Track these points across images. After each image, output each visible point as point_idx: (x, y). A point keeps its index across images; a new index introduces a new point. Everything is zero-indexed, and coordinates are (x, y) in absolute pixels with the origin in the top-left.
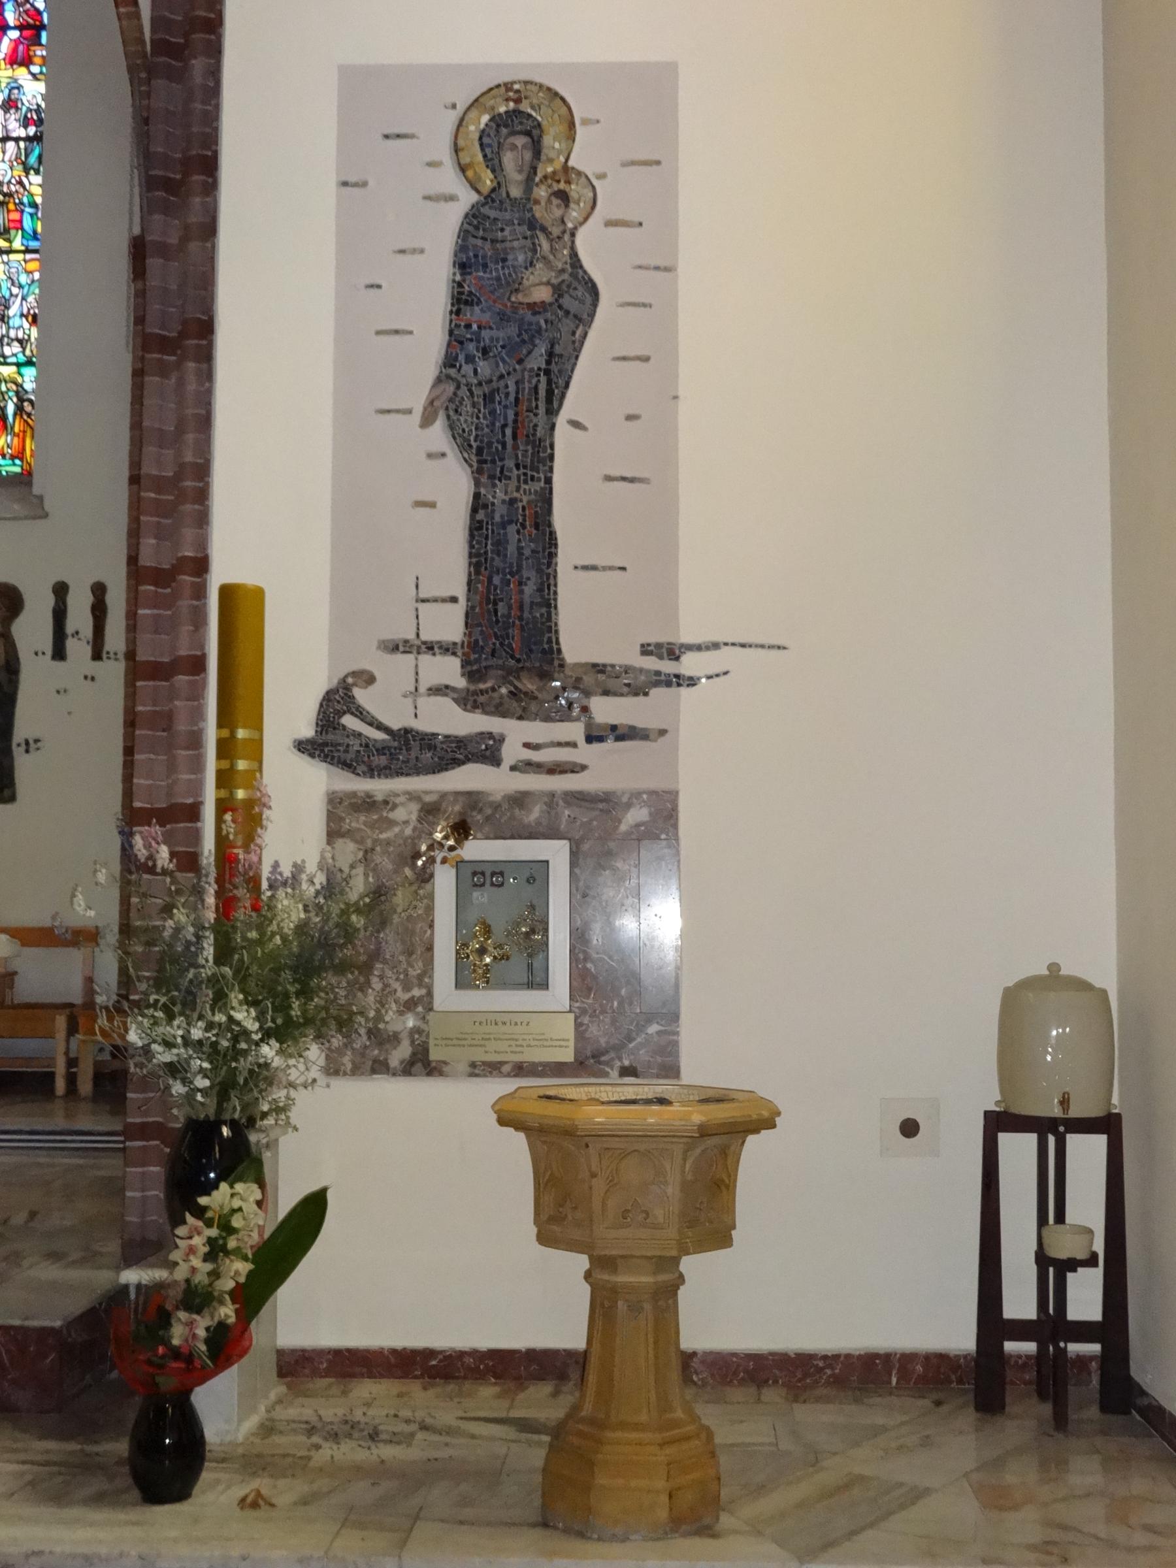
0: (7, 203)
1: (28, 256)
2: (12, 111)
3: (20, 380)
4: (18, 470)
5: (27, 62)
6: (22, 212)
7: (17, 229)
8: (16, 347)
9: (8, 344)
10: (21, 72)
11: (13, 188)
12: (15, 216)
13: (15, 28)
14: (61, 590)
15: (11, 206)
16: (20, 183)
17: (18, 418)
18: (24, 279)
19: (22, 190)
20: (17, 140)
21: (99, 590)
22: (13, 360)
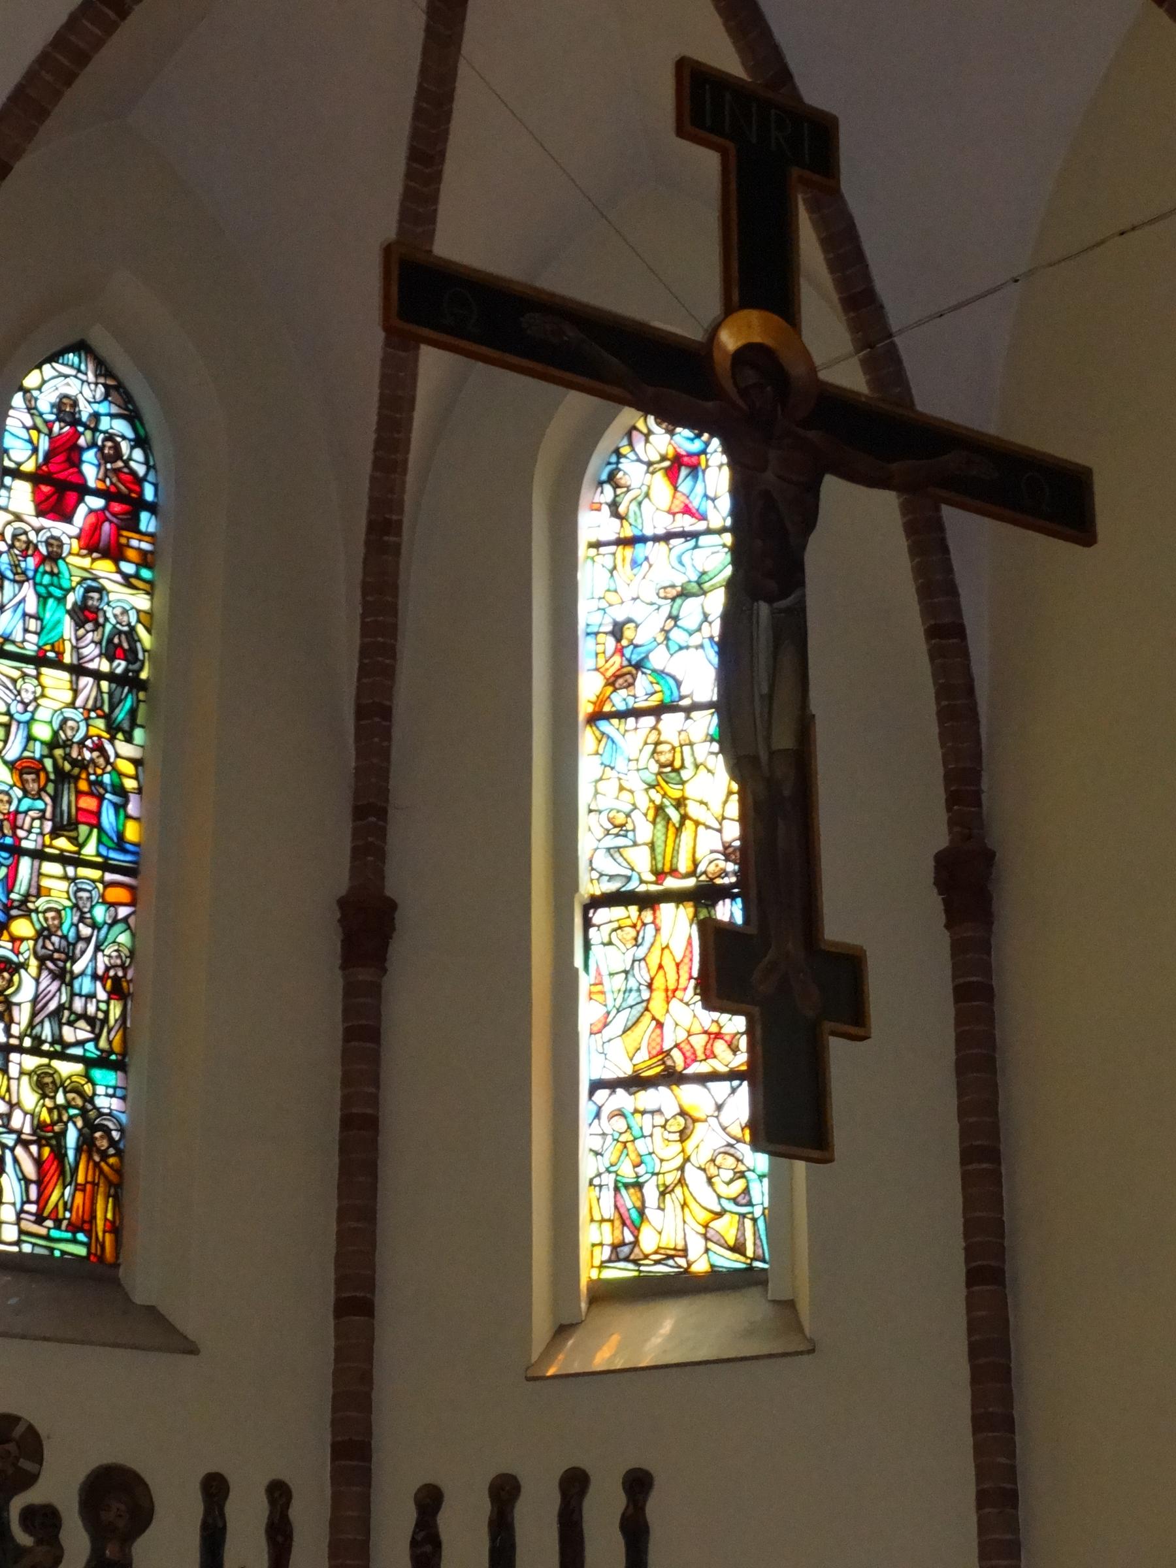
0: (77, 778)
1: (109, 877)
2: (89, 626)
3: (88, 1089)
4: (82, 1251)
5: (115, 553)
6: (101, 798)
7: (92, 826)
8: (83, 1032)
9: (70, 1023)
10: (104, 568)
11: (87, 755)
12: (88, 803)
13: (96, 493)
14: (215, 1489)
15: (83, 786)
16: (99, 748)
17: (84, 1158)
18: (100, 913)
19: (101, 761)
20: (97, 675)
21: (279, 1494)
22: (78, 1051)
